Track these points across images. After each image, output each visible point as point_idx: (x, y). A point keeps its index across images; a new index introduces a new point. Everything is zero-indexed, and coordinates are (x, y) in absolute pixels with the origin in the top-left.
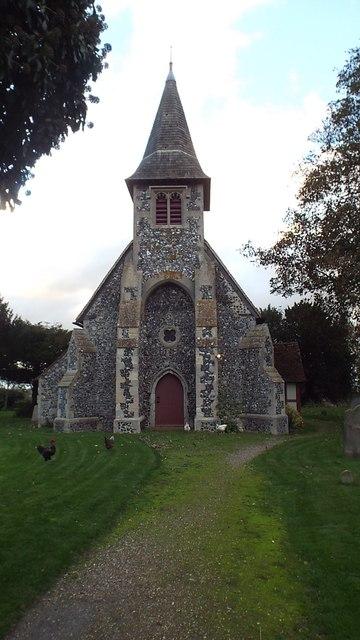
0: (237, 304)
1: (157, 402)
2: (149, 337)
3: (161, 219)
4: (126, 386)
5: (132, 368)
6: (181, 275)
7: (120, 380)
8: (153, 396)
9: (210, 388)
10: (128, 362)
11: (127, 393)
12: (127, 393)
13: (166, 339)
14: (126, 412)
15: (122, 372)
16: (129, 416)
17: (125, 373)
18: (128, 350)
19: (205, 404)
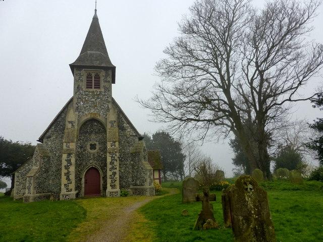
0: (129, 130)
1: (86, 183)
2: (81, 147)
3: (89, 86)
4: (68, 174)
5: (71, 164)
6: (99, 115)
7: (64, 171)
8: (83, 180)
9: (114, 174)
10: (69, 161)
11: (68, 179)
12: (68, 179)
13: (91, 149)
14: (67, 189)
15: (65, 166)
16: (69, 191)
17: (67, 167)
18: (69, 155)
19: (112, 182)
